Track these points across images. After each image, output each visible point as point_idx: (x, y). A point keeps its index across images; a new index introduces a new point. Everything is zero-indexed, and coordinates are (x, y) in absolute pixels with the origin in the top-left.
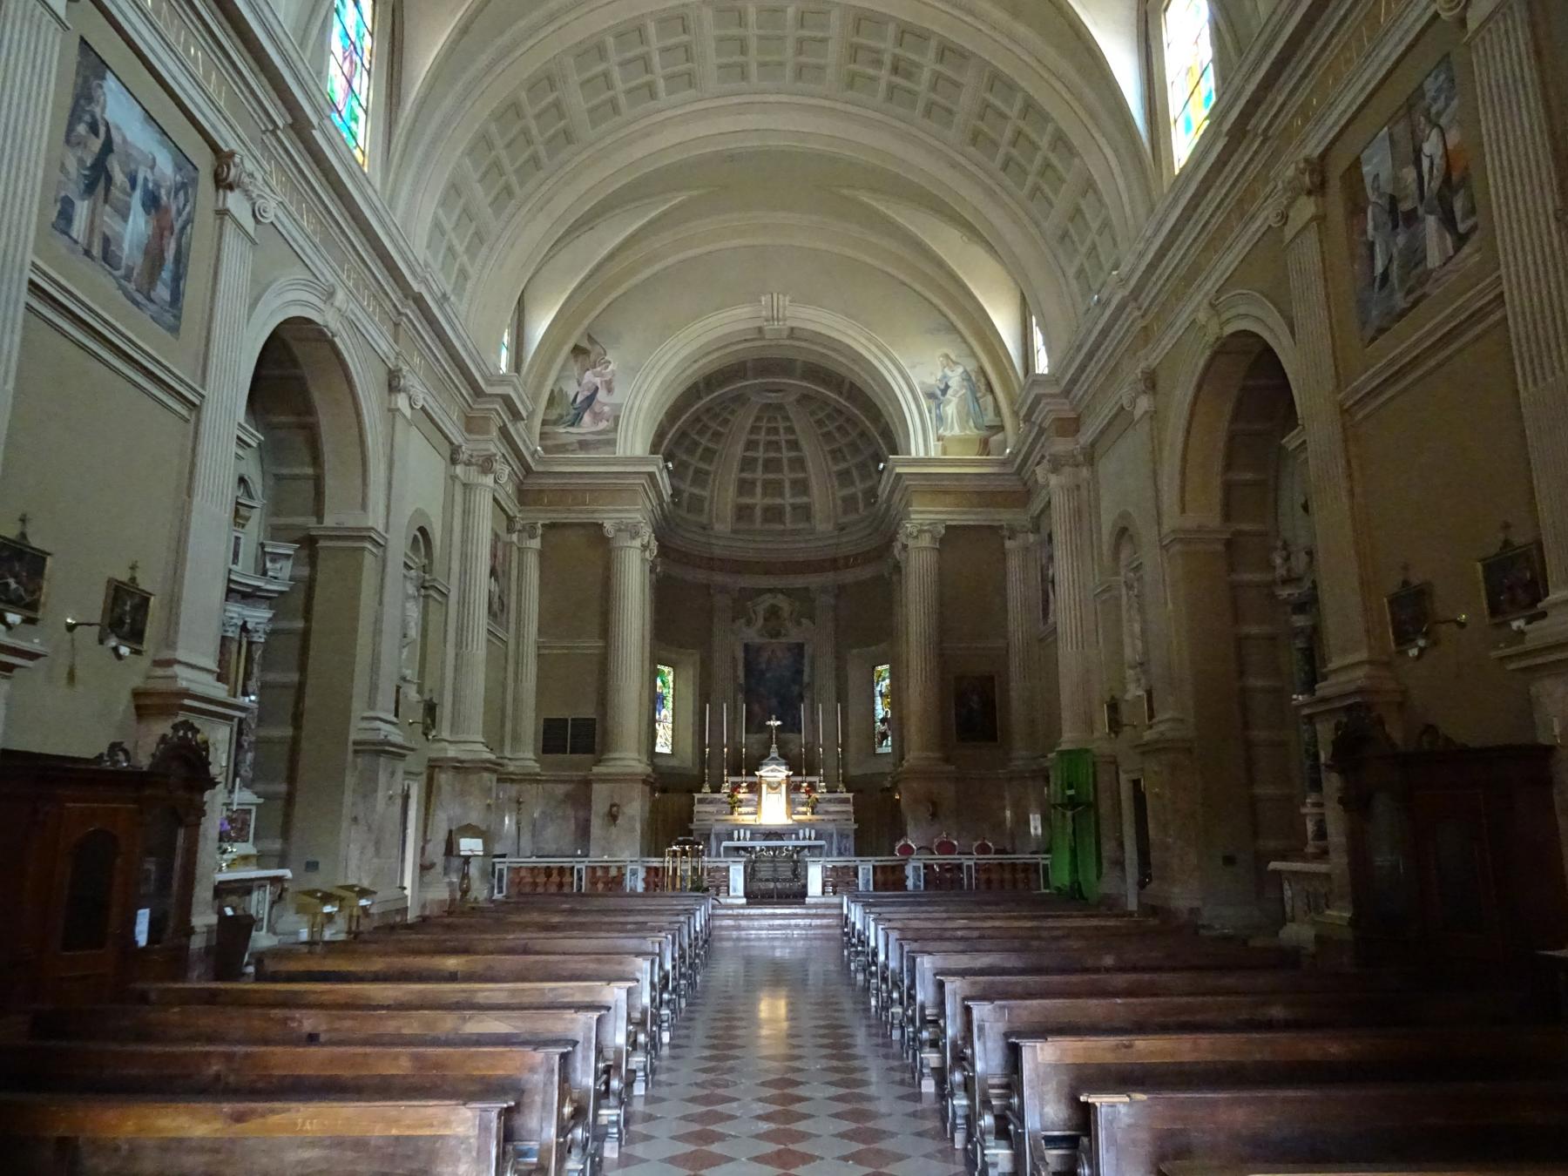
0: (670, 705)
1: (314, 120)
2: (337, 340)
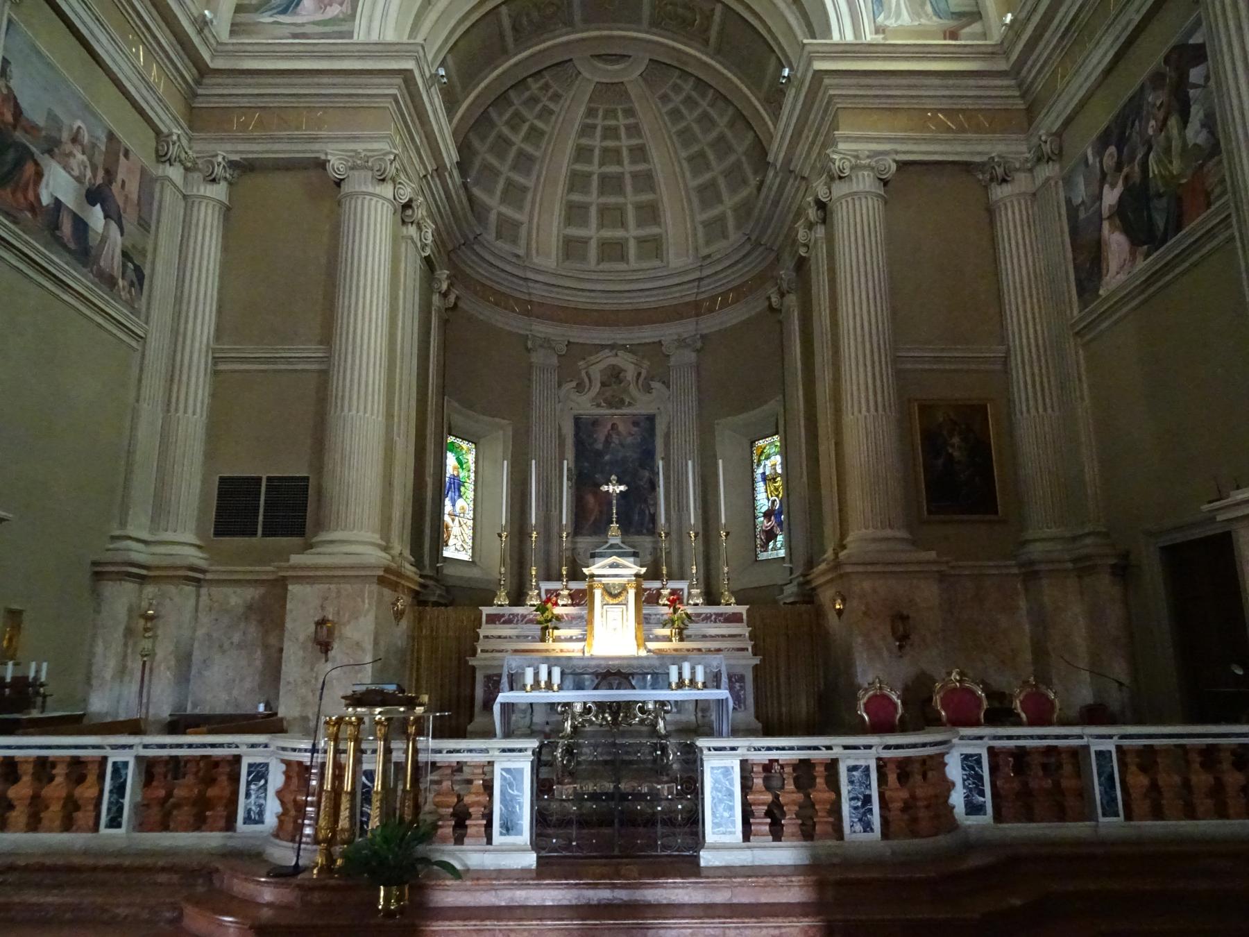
0: (470, 494)
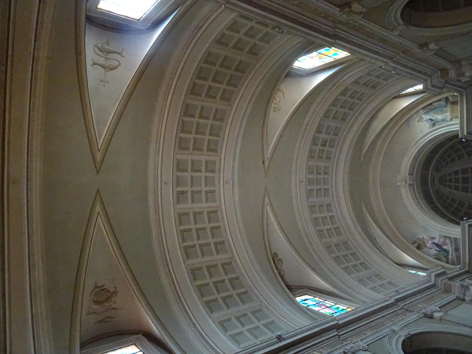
1: (335, 322)
2: (411, 333)
